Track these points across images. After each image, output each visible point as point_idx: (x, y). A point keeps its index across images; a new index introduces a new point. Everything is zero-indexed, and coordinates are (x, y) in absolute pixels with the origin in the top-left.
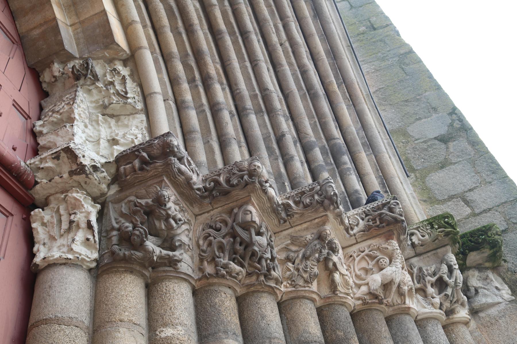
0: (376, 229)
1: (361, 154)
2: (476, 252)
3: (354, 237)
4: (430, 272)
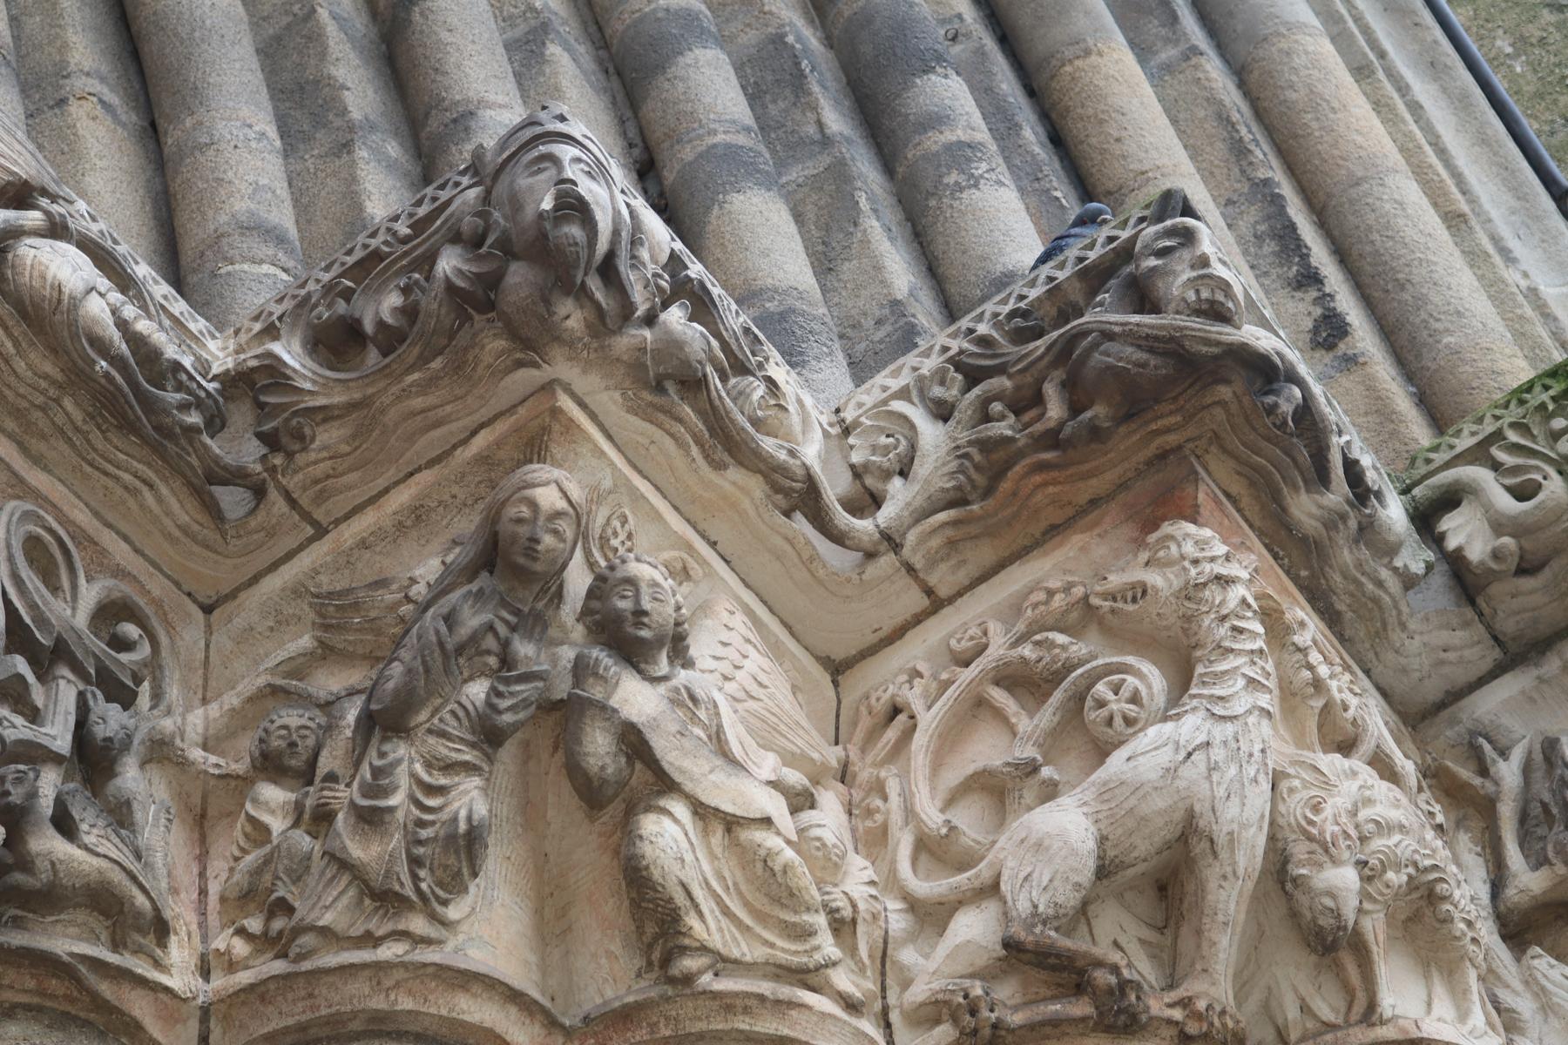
0: (1042, 467)
1: (1094, 59)
3: (887, 561)
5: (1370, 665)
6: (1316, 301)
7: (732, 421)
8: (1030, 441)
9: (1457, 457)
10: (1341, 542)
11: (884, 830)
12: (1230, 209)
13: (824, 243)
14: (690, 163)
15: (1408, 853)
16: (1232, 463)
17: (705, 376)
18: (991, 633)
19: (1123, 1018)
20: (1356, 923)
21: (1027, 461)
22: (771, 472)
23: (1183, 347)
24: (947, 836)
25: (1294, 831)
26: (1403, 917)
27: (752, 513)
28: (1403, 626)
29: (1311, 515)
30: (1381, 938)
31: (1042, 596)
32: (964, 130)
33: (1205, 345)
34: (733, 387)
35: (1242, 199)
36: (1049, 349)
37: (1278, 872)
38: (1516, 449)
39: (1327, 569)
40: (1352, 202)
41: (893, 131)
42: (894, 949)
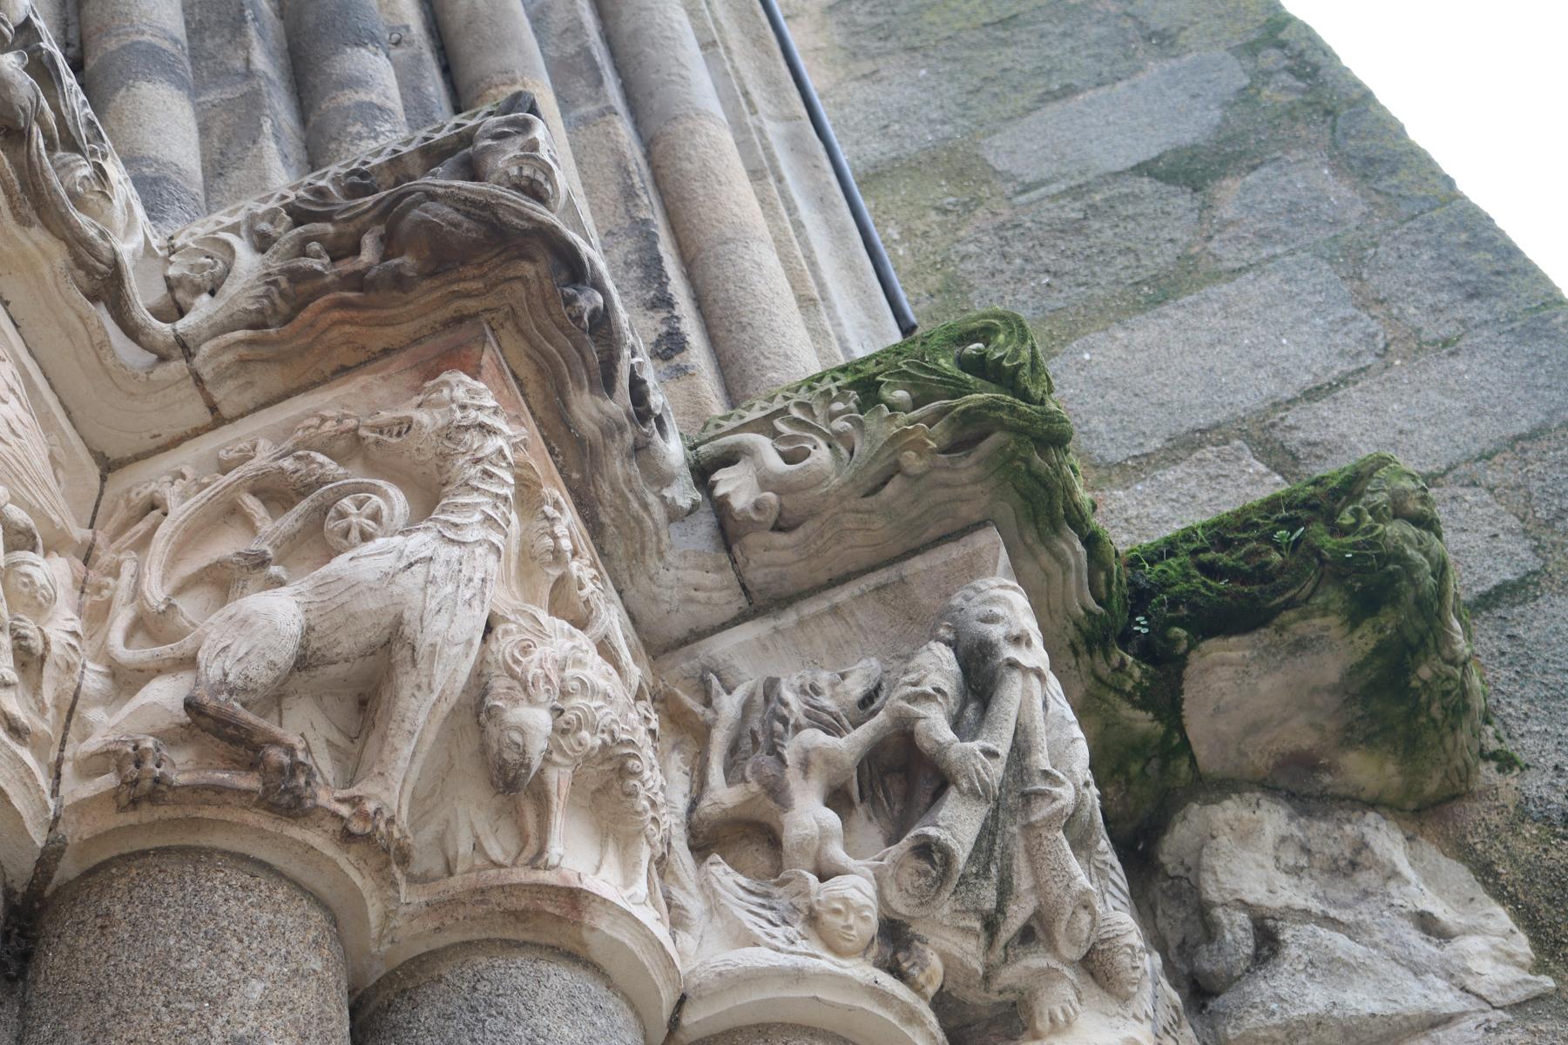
2: (1246, 639)
3: (177, 366)
4: (826, 701)
5: (623, 586)
6: (664, 321)
7: (46, 180)
8: (337, 279)
9: (744, 426)
10: (615, 452)
11: (109, 604)
12: (609, 239)
13: (222, 153)
14: (112, 52)
15: (607, 720)
16: (523, 345)
17: (30, 132)
18: (259, 449)
19: (287, 797)
20: (541, 770)
21: (331, 296)
22: (80, 249)
23: (495, 214)
24: (164, 612)
25: (499, 668)
26: (593, 787)
27: (49, 278)
28: (661, 555)
29: (592, 419)
30: (564, 791)
31: (316, 421)
32: (379, 95)
33: (517, 217)
34: (59, 158)
35: (622, 232)
36: (376, 204)
37: (477, 705)
38: (797, 422)
39: (598, 477)
40: (717, 256)
41: (315, 87)
42: (84, 706)
